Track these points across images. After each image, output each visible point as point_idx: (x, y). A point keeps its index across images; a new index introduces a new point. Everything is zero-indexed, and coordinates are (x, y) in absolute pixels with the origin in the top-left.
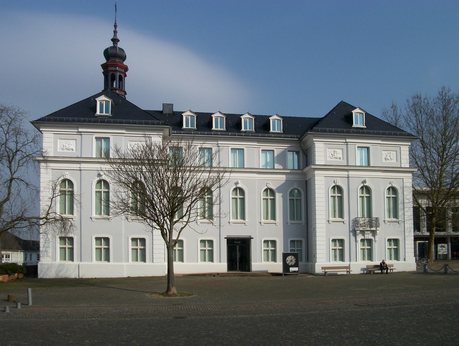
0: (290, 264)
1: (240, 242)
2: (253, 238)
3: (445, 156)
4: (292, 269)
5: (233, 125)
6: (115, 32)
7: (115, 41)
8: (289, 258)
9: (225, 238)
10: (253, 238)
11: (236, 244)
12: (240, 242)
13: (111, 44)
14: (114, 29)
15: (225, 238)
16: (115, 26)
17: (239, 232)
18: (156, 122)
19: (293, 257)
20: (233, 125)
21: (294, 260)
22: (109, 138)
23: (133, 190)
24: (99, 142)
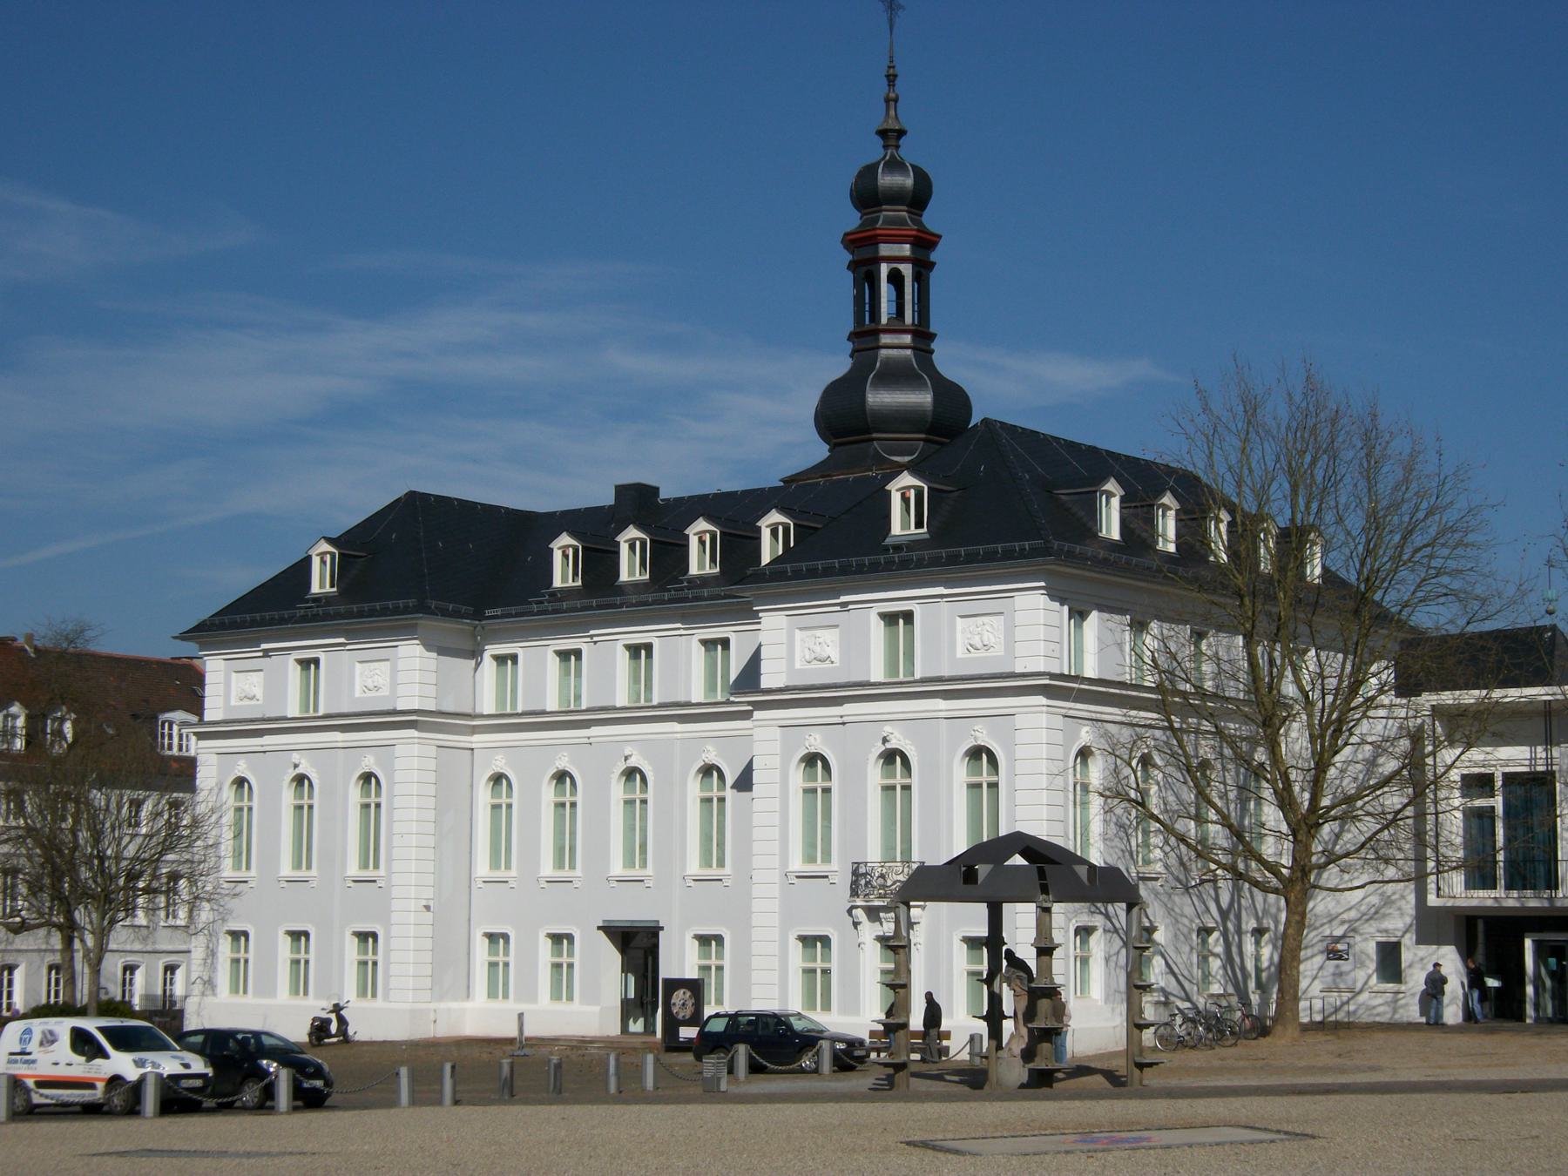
7: (891, 136)
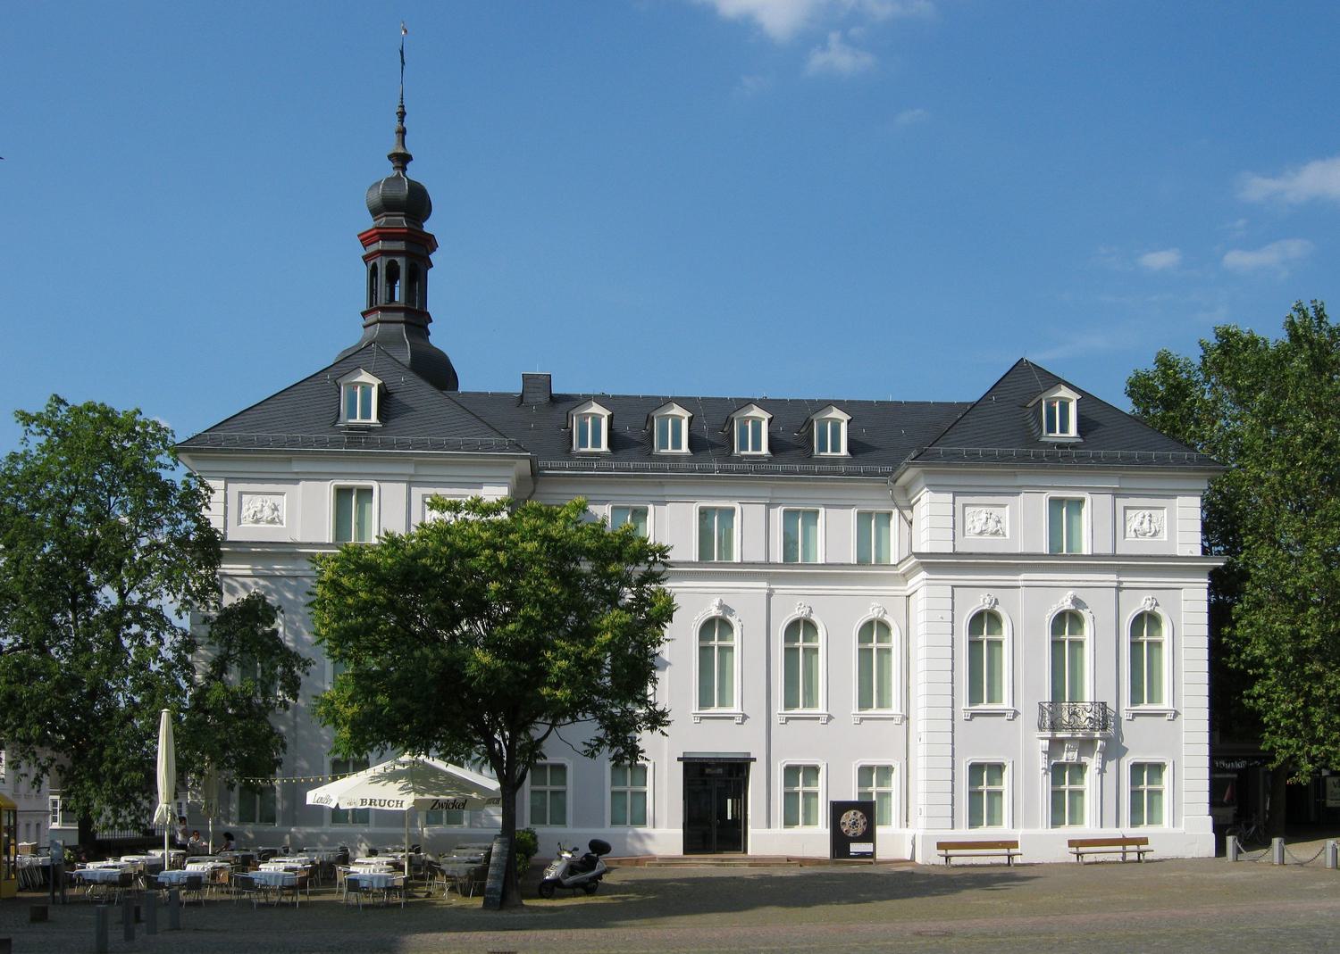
0: (850, 834)
1: (720, 771)
2: (754, 760)
3: (1260, 501)
4: (855, 848)
5: (794, 441)
6: (402, 132)
8: (848, 818)
9: (679, 759)
10: (754, 760)
11: (709, 775)
12: (720, 771)
13: (389, 170)
14: (398, 124)
15: (679, 759)
16: (402, 115)
17: (717, 742)
18: (495, 439)
19: (859, 814)
20: (794, 441)
21: (861, 822)
22: (370, 491)
23: (405, 735)
24: (225, 556)
